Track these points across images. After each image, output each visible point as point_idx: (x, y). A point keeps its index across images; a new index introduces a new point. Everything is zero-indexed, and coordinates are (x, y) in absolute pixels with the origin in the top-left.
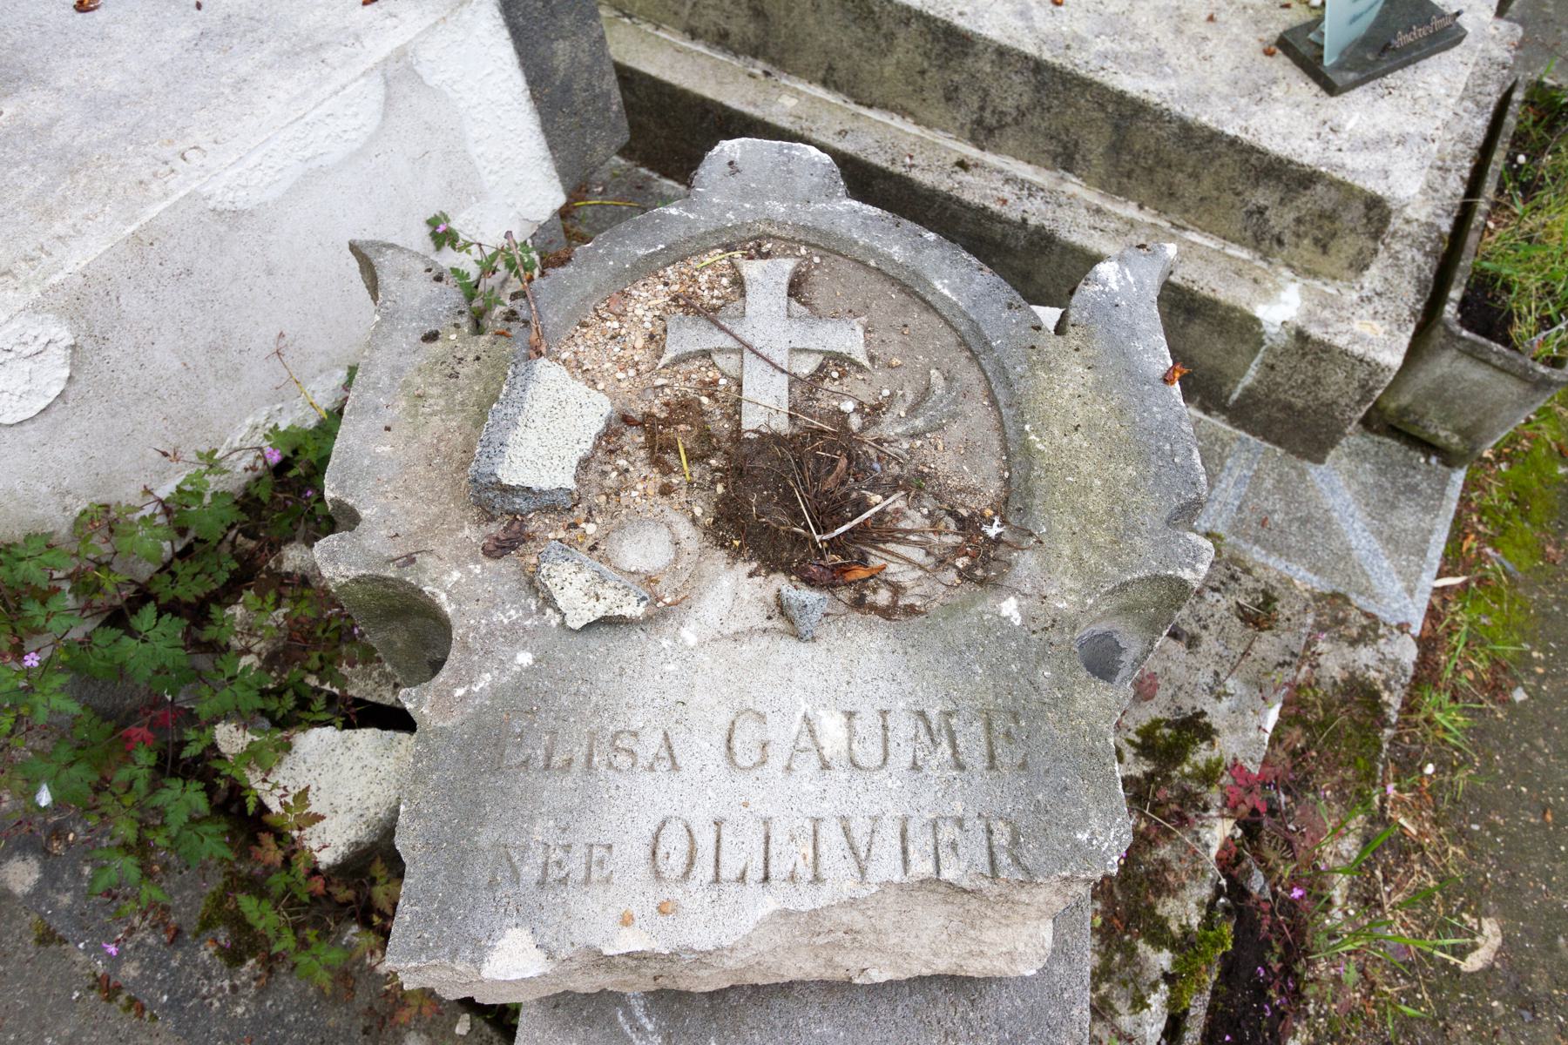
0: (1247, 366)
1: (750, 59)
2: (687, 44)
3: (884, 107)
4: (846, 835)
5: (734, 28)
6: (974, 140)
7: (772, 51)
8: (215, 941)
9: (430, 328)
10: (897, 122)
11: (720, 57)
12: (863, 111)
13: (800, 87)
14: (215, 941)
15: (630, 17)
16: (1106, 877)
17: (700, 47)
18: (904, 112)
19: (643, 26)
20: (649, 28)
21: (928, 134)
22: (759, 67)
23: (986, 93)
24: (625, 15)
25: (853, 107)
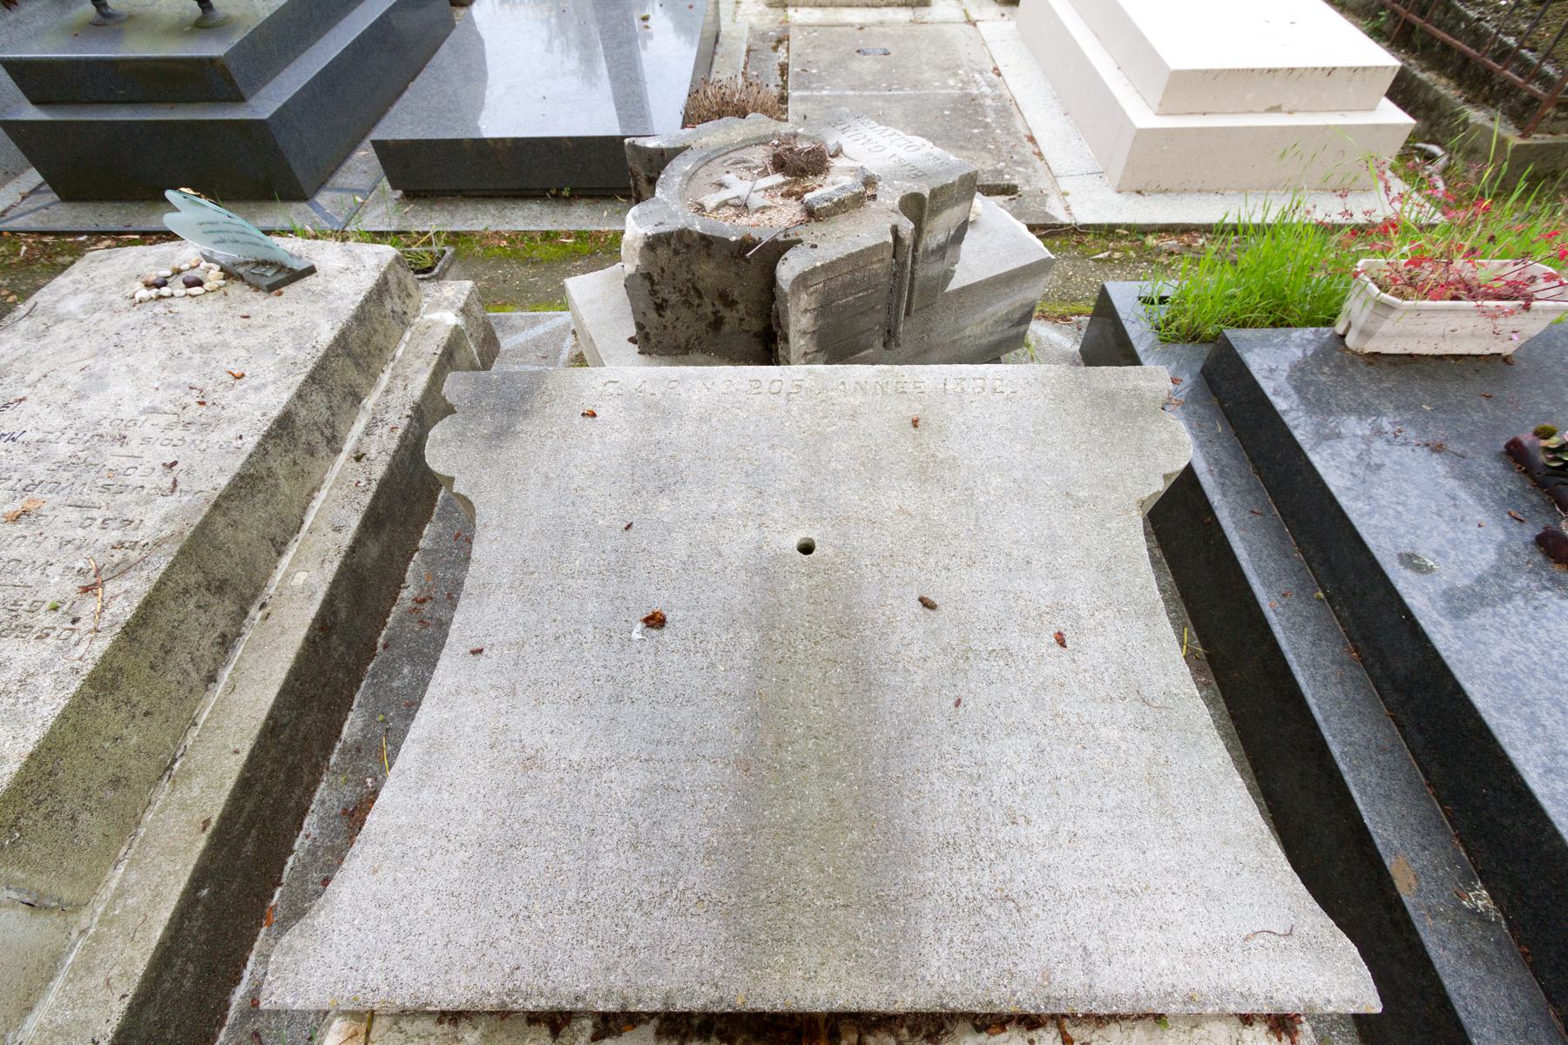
0: (401, 621)
1: (246, 621)
2: (220, 688)
3: (305, 509)
4: (782, 75)
5: (222, 624)
6: (338, 451)
7: (248, 592)
8: (1292, 409)
9: (631, 531)
10: (316, 504)
11: (239, 653)
12: (305, 527)
13: (278, 578)
14: (1292, 409)
15: (174, 761)
16: (1500, 546)
17: (225, 675)
18: (310, 496)
19: (189, 742)
20: (195, 732)
21: (327, 484)
22: (255, 613)
23: (315, 423)
24: (170, 768)
25: (301, 535)
